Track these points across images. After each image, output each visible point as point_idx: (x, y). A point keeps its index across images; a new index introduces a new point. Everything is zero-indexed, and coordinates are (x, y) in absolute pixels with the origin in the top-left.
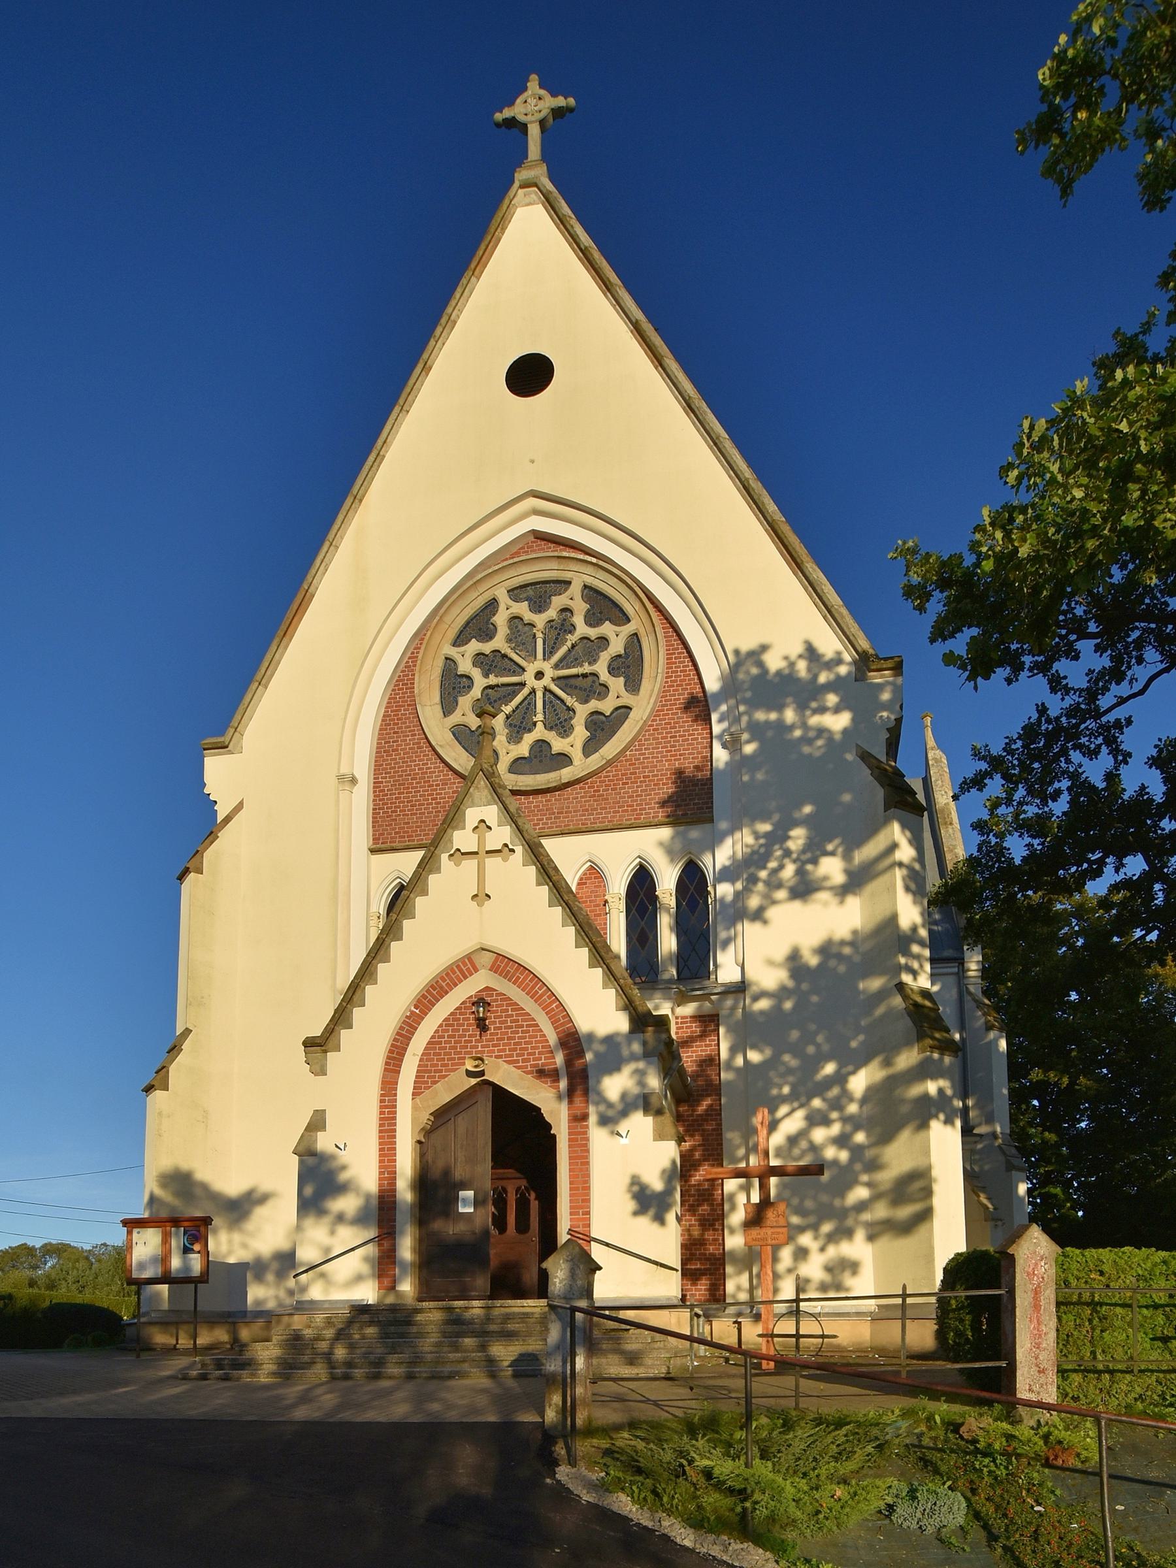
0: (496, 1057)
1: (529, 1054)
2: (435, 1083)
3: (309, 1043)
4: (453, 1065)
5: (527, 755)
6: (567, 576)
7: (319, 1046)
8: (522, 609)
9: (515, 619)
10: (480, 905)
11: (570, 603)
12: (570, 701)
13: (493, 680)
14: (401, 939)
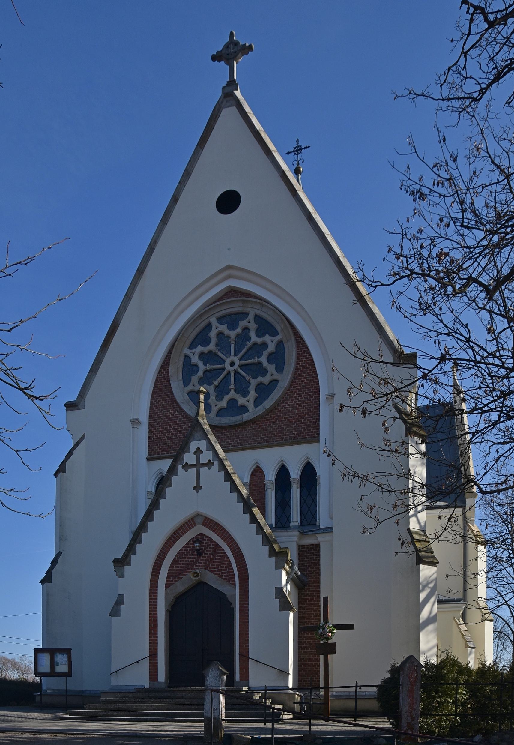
0: (205, 569)
1: (221, 567)
2: (176, 581)
3: (117, 562)
4: (184, 572)
5: (226, 406)
6: (247, 310)
7: (121, 563)
8: (223, 328)
9: (220, 334)
10: (197, 492)
11: (248, 324)
12: (248, 377)
13: (209, 367)
14: (159, 509)
